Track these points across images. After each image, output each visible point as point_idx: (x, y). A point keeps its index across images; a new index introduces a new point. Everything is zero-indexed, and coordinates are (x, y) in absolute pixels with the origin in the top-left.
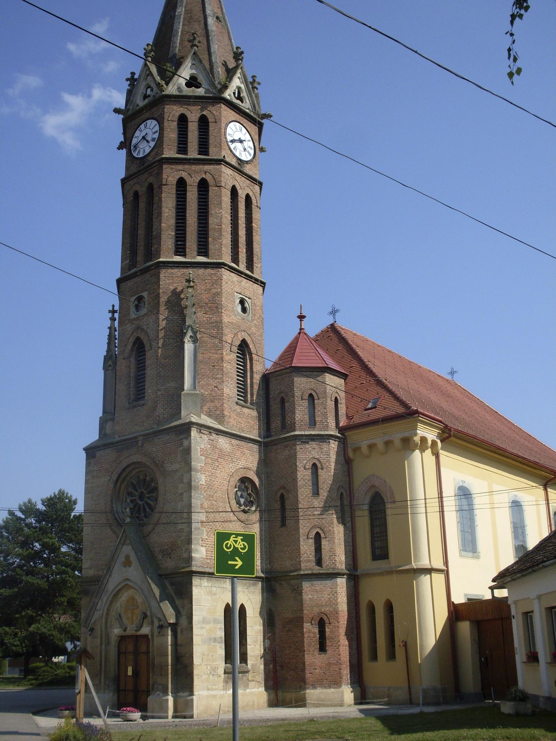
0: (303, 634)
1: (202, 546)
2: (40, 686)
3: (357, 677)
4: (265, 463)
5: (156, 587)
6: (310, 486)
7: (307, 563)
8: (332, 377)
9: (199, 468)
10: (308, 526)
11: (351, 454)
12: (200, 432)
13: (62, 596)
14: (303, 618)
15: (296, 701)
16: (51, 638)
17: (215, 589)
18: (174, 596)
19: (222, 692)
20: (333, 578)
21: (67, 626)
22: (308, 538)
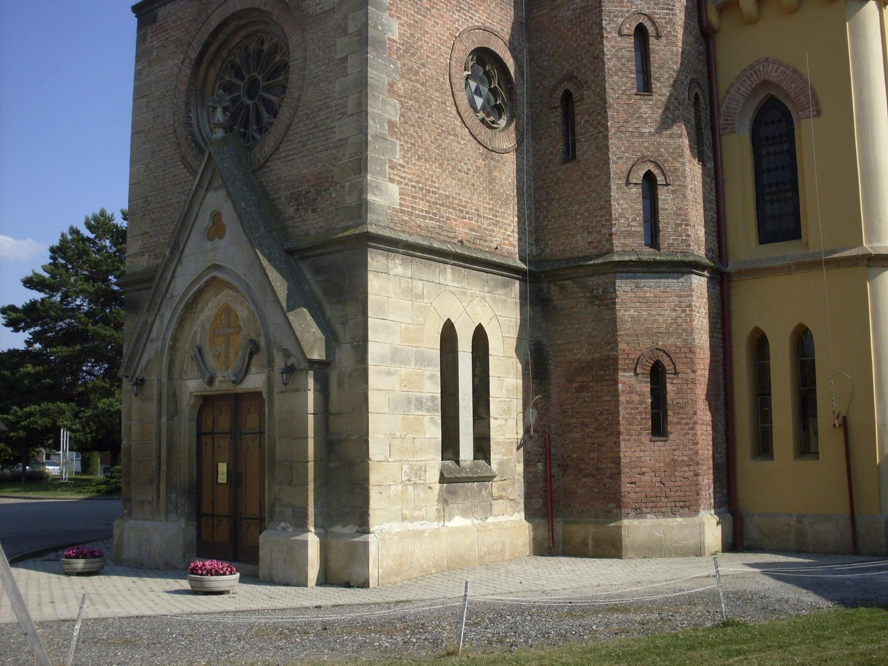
0: (618, 396)
1: (392, 180)
3: (725, 492)
5: (279, 277)
6: (631, 73)
7: (625, 238)
10: (628, 159)
11: (712, 16)
14: (616, 360)
15: (597, 546)
17: (419, 284)
18: (322, 298)
19: (435, 525)
20: (683, 273)
22: (628, 183)
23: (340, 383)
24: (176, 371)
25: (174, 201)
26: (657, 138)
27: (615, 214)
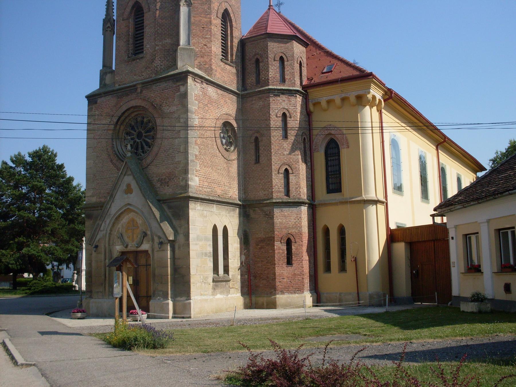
1: (196, 176)
2: (33, 294)
4: (241, 111)
8: (298, 44)
9: (194, 110)
10: (279, 164)
11: (311, 108)
12: (195, 80)
13: (48, 226)
14: (274, 237)
15: (267, 305)
16: (40, 258)
17: (205, 212)
18: (172, 218)
19: (211, 297)
20: (298, 206)
21: (52, 249)
22: (278, 173)
23: (179, 248)
24: (111, 242)
25: (107, 176)
26: (290, 156)
27: (274, 184)
